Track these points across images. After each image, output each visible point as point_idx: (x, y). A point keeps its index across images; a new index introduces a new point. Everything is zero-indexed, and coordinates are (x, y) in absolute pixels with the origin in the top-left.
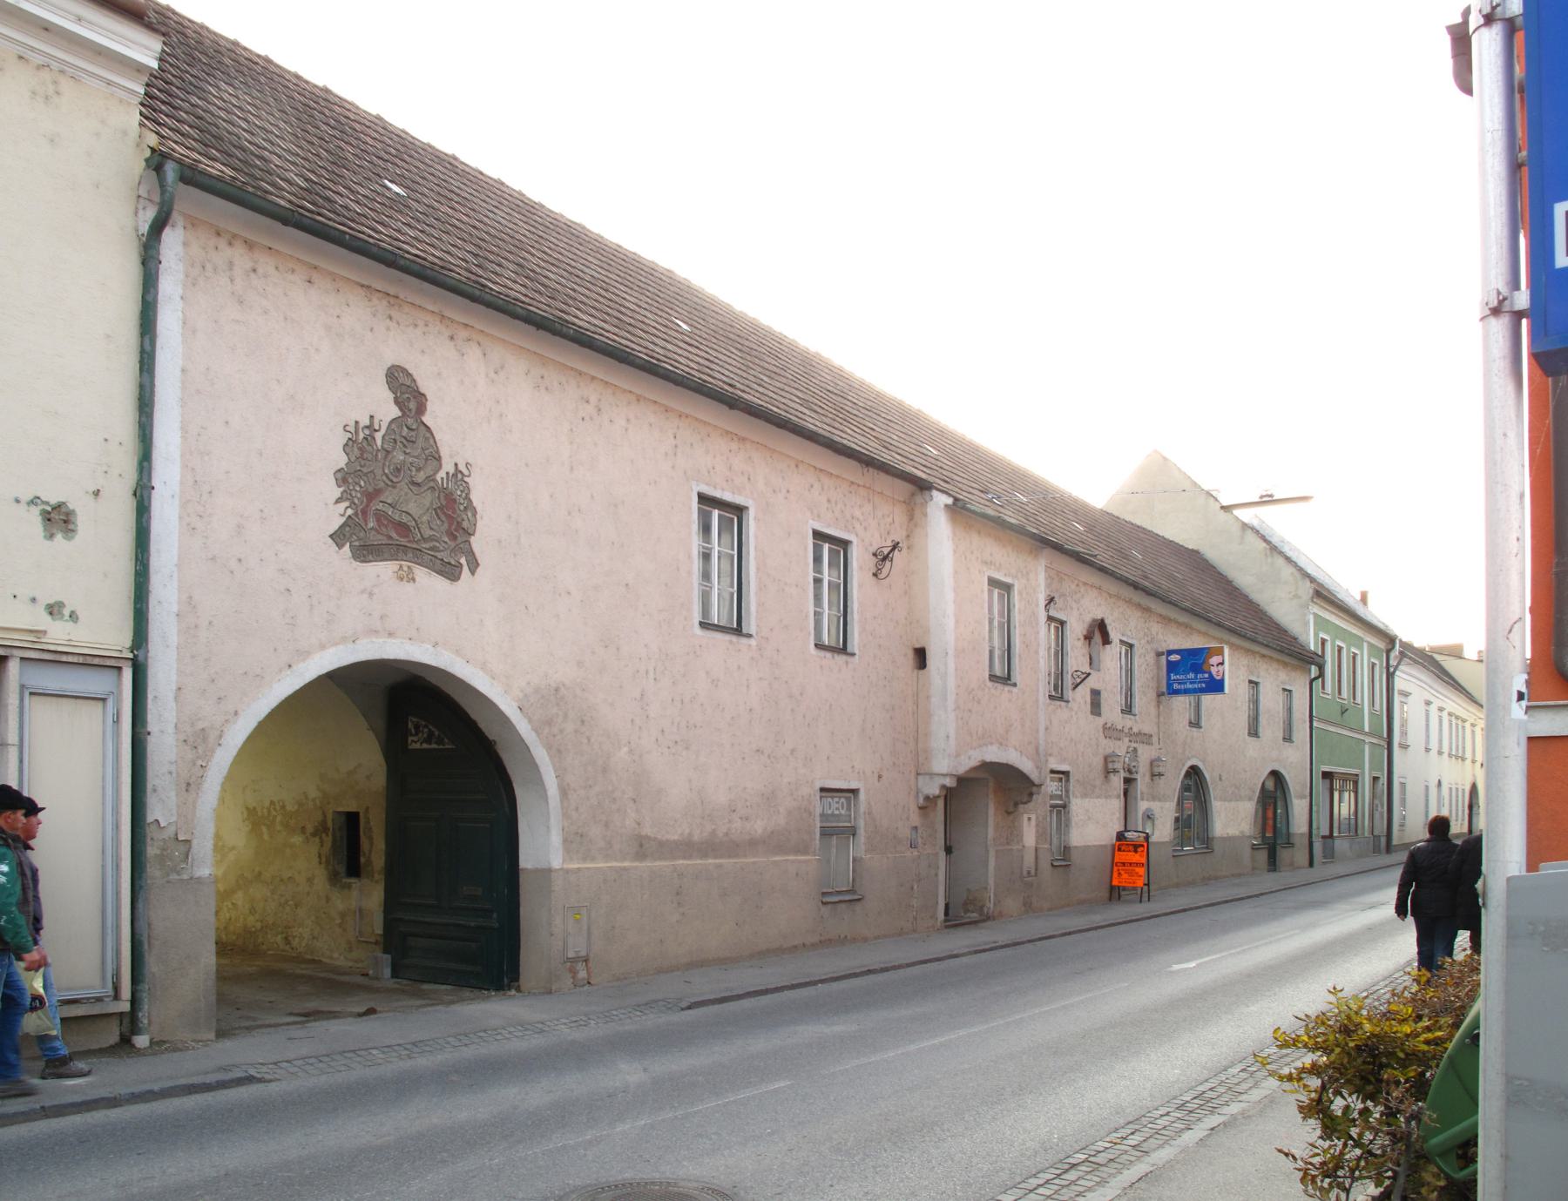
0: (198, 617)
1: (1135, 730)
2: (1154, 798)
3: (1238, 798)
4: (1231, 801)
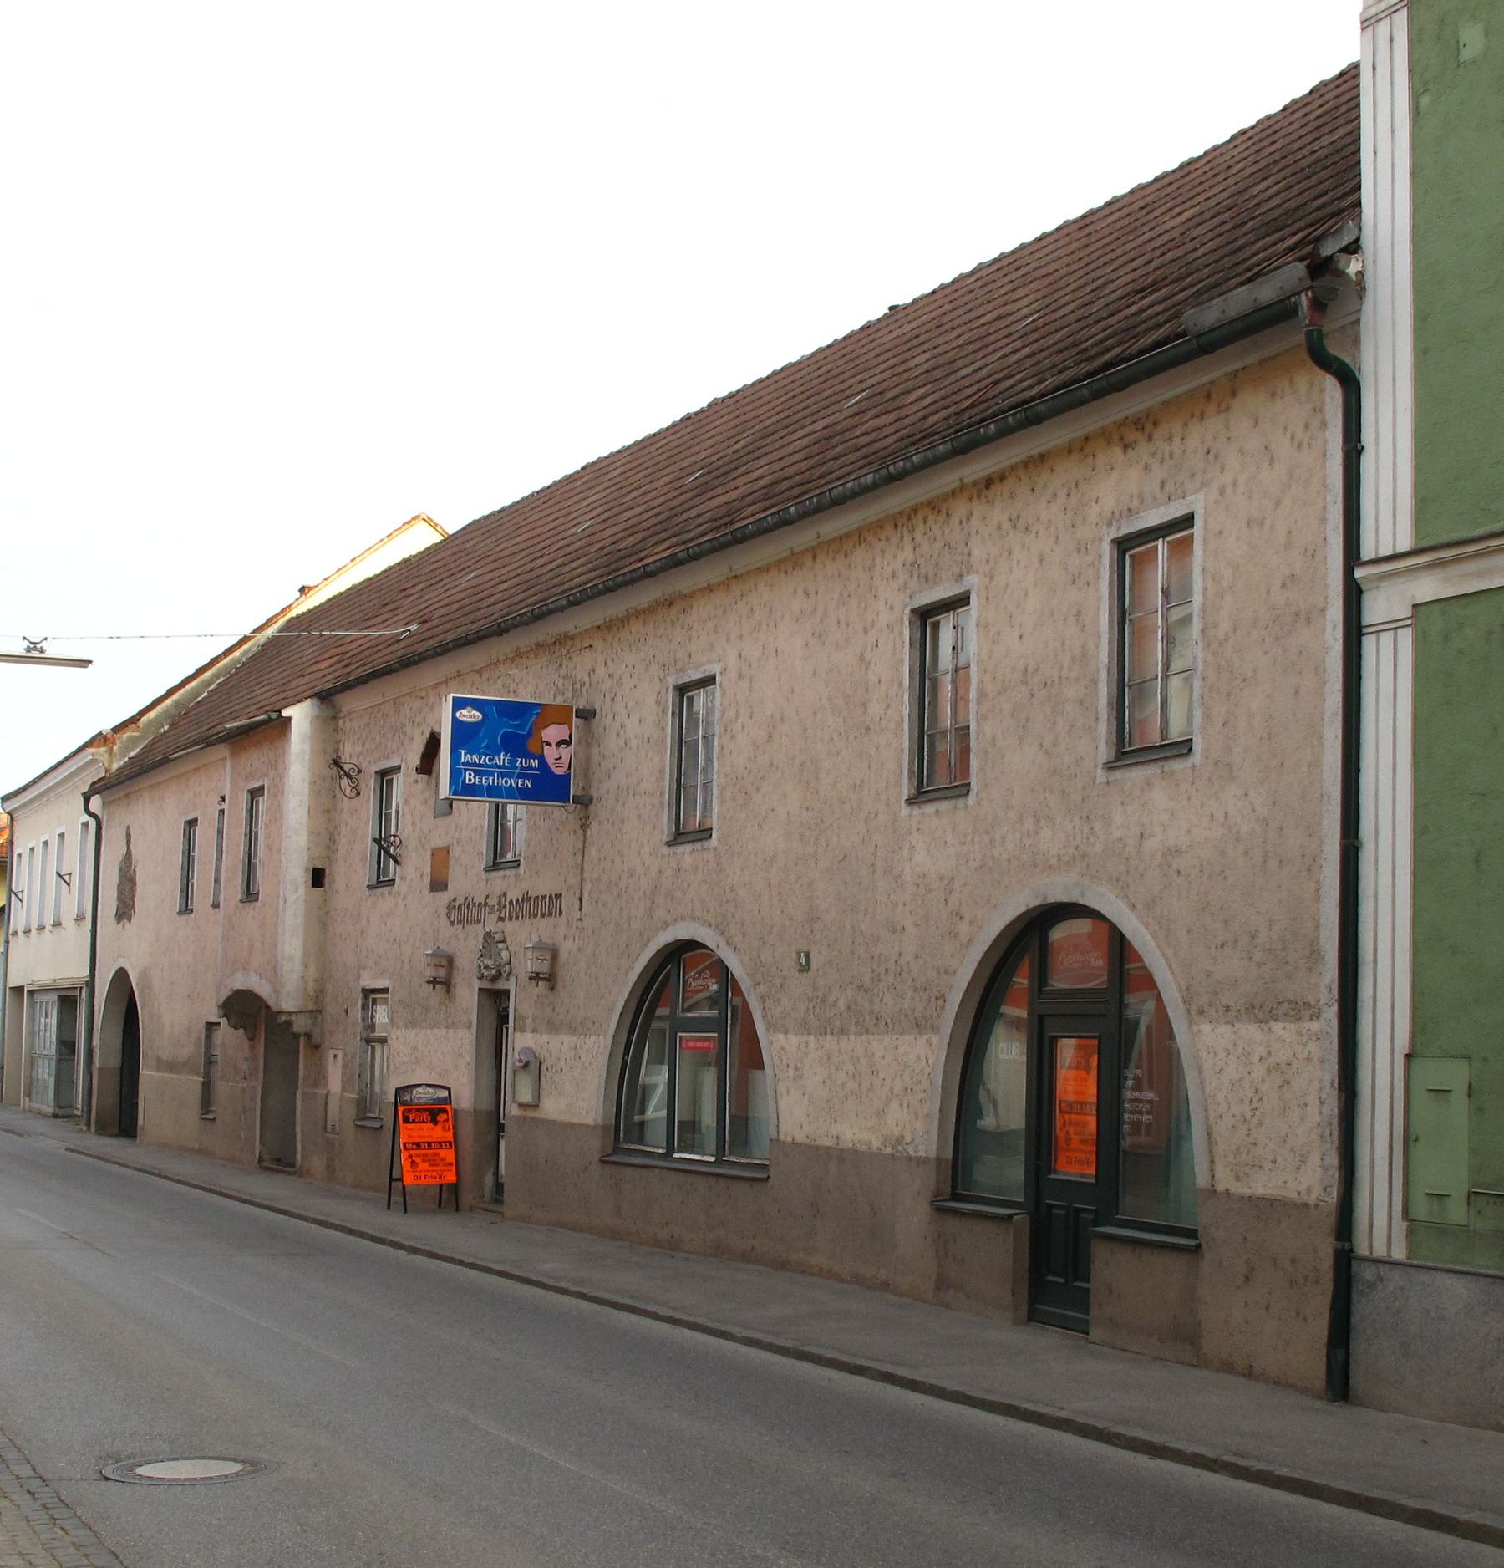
0: (1120, 873)
1: (514, 895)
2: (553, 1028)
3: (864, 1021)
4: (843, 1031)
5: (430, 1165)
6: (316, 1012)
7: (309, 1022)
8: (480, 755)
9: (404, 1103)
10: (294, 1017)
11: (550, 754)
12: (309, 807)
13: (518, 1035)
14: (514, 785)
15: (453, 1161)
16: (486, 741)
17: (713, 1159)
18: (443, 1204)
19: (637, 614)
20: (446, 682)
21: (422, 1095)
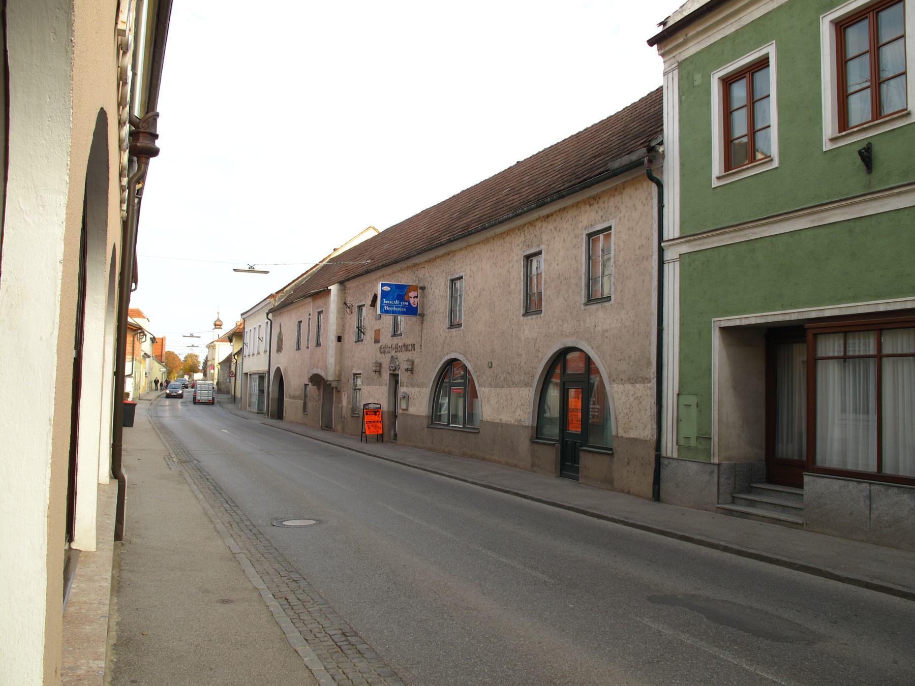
1: (400, 344)
2: (412, 386)
4: (503, 387)
6: (339, 381)
9: (366, 409)
10: (332, 382)
11: (411, 300)
13: (401, 388)
21: (372, 407)
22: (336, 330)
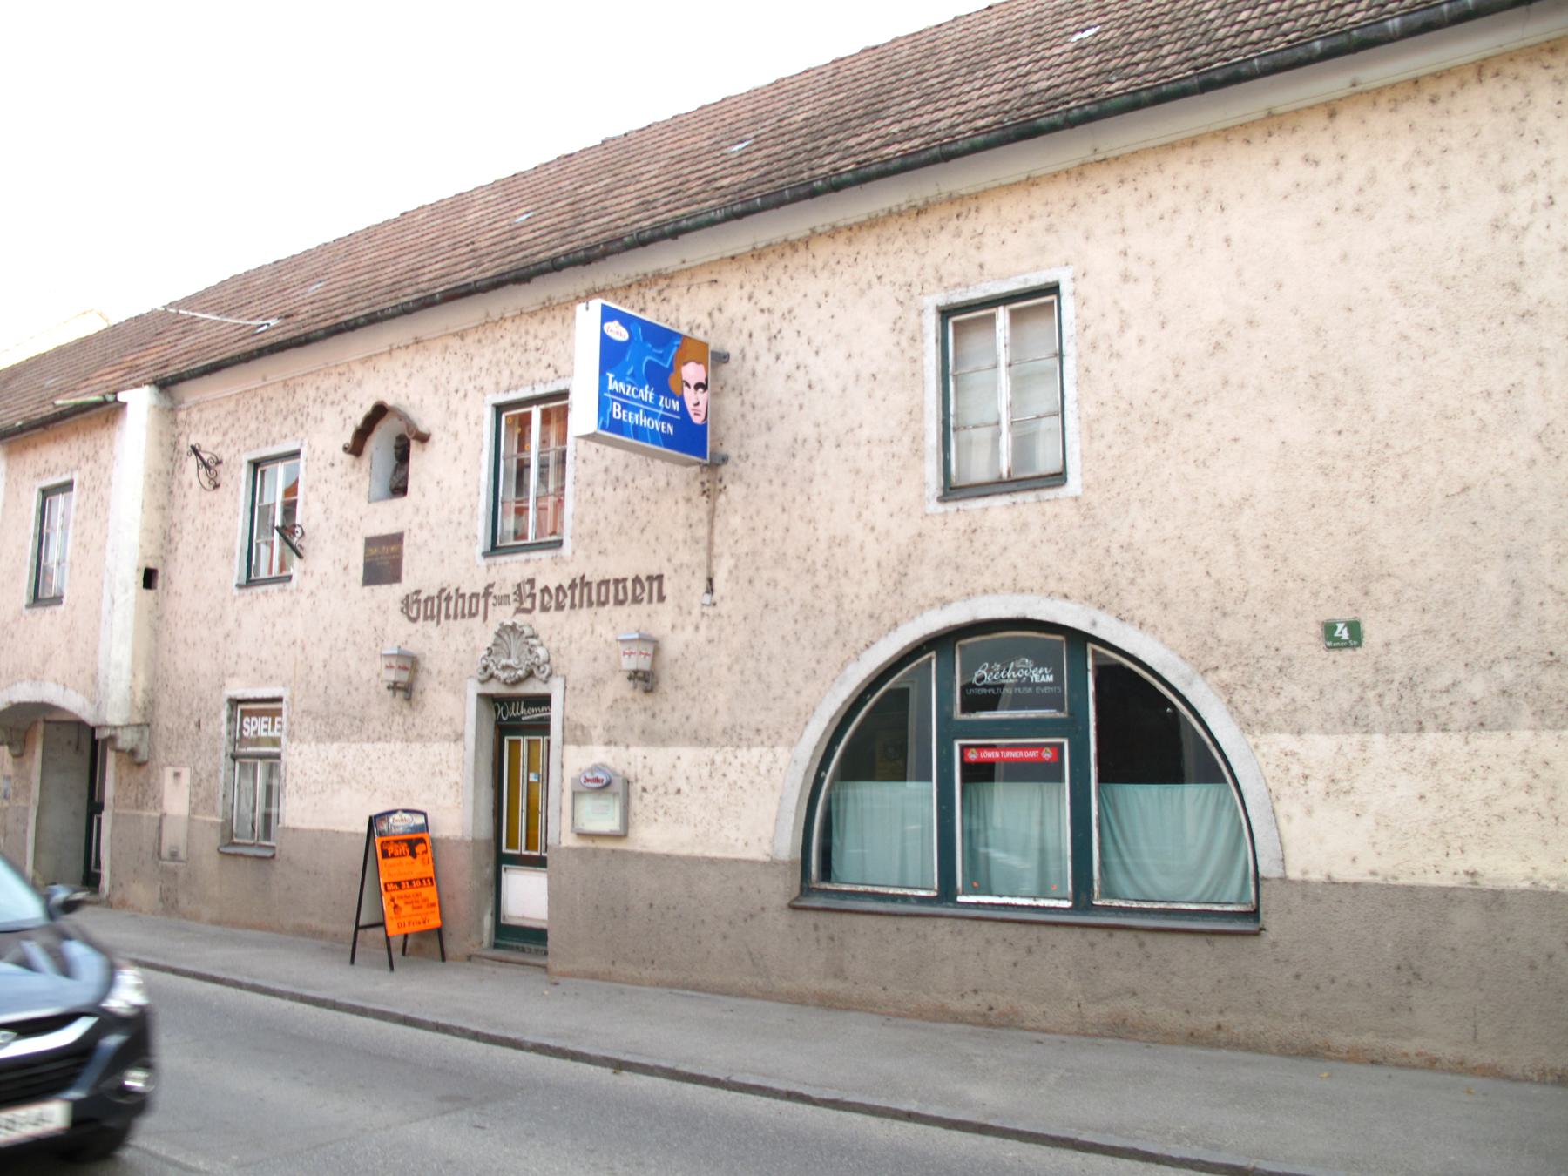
2: (649, 737)
5: (414, 908)
6: (145, 725)
7: (136, 736)
8: (627, 383)
9: (381, 834)
10: (119, 732)
11: (690, 396)
12: (143, 501)
13: (571, 750)
14: (658, 429)
15: (436, 900)
16: (631, 369)
17: (1067, 904)
18: (407, 951)
19: (834, 232)
20: (390, 352)
21: (399, 824)
22: (141, 546)
